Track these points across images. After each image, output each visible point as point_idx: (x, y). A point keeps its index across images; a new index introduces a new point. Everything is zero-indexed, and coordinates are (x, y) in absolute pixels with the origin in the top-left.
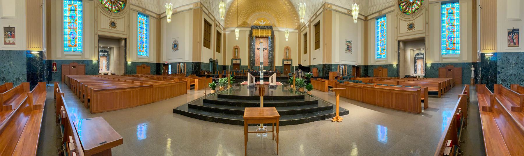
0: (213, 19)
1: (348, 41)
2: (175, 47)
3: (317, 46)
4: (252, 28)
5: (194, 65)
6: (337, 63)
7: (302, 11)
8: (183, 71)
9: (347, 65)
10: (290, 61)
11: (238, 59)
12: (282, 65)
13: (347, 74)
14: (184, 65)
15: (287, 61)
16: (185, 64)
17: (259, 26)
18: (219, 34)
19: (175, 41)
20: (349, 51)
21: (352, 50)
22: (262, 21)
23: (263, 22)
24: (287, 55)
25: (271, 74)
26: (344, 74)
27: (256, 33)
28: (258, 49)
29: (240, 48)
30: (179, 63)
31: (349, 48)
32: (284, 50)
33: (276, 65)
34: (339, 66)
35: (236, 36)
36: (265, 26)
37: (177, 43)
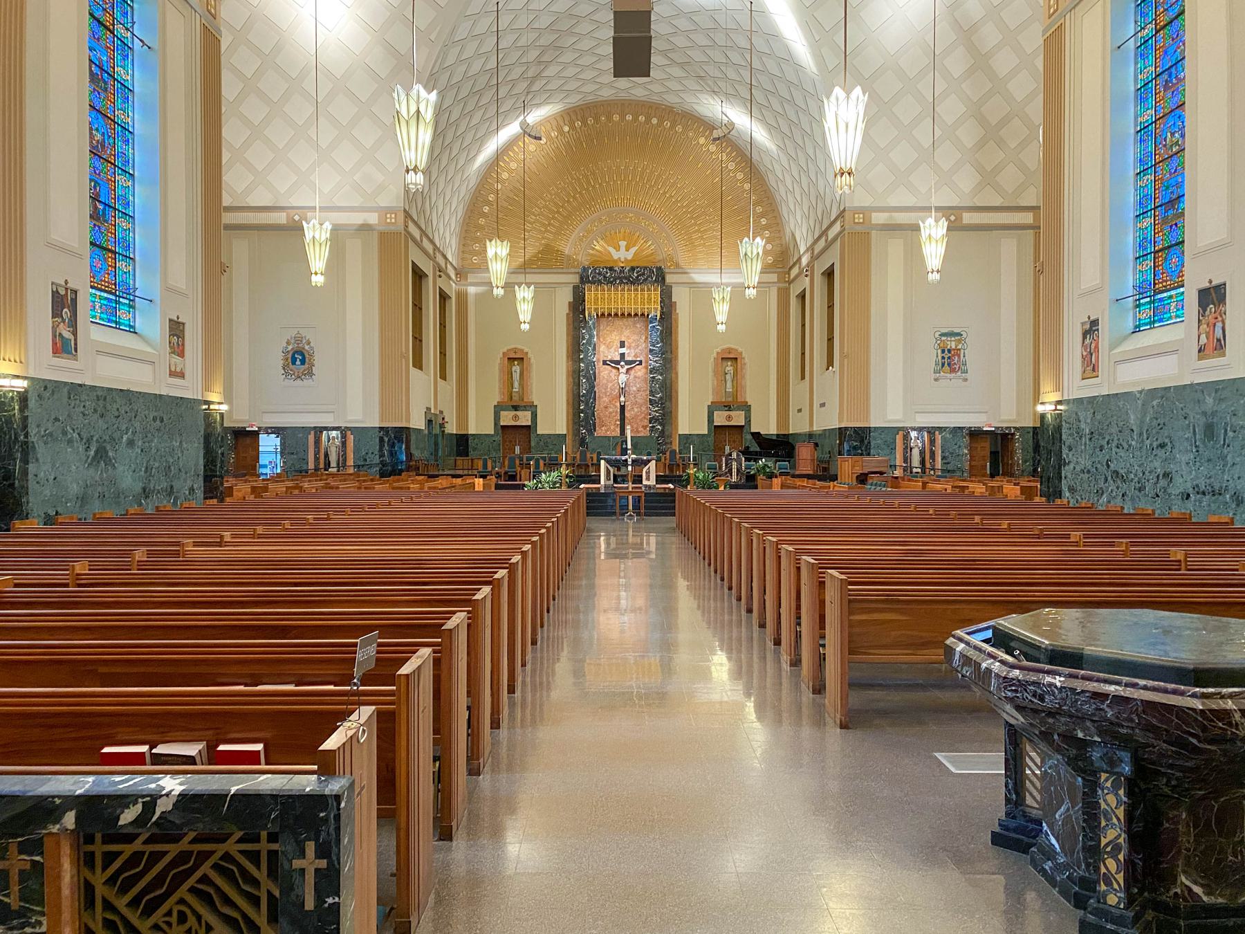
2: (298, 362)
3: (830, 363)
4: (584, 279)
5: (386, 439)
7: (749, 264)
8: (333, 464)
9: (940, 429)
11: (525, 408)
12: (706, 432)
13: (939, 464)
14: (344, 436)
15: (728, 413)
16: (349, 433)
17: (611, 269)
18: (444, 297)
19: (299, 339)
20: (953, 371)
22: (623, 244)
23: (627, 250)
26: (928, 465)
27: (596, 298)
28: (605, 363)
30: (319, 430)
31: (950, 360)
32: (716, 365)
33: (680, 432)
34: (901, 433)
35: (522, 318)
36: (633, 269)
37: (307, 347)
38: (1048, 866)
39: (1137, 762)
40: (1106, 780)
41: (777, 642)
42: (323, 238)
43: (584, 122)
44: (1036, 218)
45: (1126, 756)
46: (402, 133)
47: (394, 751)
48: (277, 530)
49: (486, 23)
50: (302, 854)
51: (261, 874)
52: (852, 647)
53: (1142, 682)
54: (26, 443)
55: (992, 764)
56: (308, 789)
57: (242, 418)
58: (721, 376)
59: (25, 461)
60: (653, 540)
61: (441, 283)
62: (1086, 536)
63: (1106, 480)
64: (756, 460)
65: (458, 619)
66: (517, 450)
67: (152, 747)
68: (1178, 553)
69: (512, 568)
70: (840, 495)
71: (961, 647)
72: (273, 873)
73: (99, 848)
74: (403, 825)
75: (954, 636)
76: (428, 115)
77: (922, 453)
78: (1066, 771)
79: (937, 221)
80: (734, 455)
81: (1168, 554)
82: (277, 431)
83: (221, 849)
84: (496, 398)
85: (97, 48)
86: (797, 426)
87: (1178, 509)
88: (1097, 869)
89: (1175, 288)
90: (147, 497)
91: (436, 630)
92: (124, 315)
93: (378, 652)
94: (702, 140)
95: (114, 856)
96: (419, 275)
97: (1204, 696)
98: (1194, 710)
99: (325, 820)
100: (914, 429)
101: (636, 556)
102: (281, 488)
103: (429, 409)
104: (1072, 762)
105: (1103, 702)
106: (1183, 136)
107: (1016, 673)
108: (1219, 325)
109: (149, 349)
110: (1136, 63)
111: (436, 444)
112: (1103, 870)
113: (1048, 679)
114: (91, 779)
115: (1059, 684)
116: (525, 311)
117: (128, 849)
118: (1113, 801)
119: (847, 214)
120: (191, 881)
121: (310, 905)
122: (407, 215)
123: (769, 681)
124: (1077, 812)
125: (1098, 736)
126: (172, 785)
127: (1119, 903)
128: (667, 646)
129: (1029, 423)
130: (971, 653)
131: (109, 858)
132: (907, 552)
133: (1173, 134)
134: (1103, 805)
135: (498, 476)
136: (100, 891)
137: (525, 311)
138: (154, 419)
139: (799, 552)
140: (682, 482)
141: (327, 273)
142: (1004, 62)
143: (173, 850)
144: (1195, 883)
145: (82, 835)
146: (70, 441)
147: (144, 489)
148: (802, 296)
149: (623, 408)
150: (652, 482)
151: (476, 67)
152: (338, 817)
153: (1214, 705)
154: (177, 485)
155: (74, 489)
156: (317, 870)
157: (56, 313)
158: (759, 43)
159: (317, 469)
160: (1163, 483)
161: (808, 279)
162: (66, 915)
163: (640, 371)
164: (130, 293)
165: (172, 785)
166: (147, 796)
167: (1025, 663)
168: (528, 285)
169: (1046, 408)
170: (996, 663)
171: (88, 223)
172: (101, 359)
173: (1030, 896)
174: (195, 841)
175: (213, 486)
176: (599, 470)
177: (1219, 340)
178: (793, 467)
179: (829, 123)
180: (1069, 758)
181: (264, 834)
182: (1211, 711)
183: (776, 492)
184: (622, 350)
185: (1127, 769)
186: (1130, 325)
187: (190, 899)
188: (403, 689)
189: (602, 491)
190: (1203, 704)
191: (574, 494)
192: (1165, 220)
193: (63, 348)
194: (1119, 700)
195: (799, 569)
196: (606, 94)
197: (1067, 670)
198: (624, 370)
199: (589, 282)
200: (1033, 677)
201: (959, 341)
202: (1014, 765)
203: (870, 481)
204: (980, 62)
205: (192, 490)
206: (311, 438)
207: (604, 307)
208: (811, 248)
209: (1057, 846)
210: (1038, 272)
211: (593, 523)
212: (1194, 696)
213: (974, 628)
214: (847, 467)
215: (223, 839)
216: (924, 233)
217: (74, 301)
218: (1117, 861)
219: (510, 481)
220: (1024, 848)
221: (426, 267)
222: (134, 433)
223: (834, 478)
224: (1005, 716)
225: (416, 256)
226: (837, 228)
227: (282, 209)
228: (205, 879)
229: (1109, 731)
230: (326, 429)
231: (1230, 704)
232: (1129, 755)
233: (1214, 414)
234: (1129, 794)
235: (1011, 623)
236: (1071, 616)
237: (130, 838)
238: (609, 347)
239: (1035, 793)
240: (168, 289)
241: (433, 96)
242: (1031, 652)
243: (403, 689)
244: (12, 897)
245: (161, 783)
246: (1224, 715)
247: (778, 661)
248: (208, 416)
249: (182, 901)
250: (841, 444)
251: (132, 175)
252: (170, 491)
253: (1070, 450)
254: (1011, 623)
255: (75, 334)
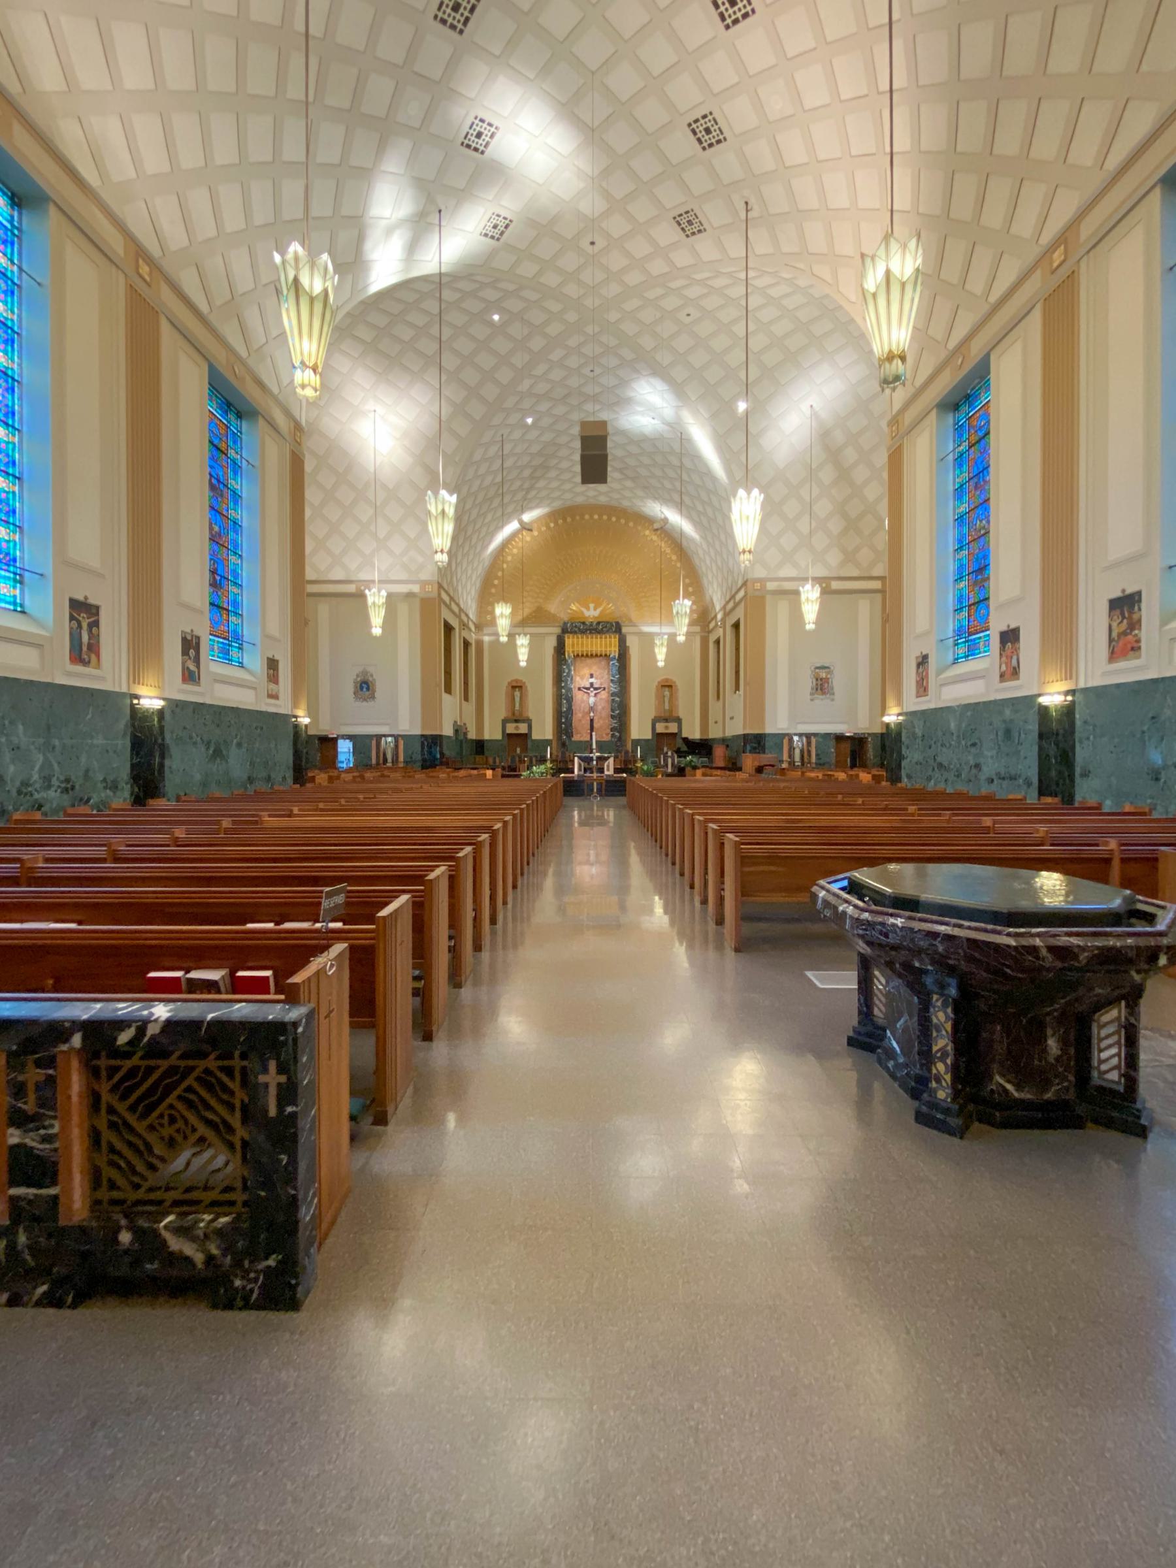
0: (117, 244)
1: (818, 665)
3: (737, 688)
4: (565, 630)
6: (782, 729)
8: (390, 760)
10: (676, 724)
11: (523, 721)
13: (814, 759)
14: (396, 741)
17: (584, 623)
18: (466, 644)
19: (365, 673)
21: (836, 690)
22: (592, 606)
23: (595, 609)
24: (667, 707)
25: (606, 759)
26: (806, 760)
27: (573, 644)
28: (579, 689)
29: (529, 687)
30: (379, 737)
31: (822, 686)
36: (599, 623)
37: (371, 679)
38: (891, 1064)
39: (961, 987)
40: (937, 1000)
41: (692, 887)
42: (381, 603)
43: (565, 520)
44: (884, 585)
45: (953, 982)
46: (432, 528)
47: (374, 976)
48: (335, 806)
49: (493, 450)
50: (265, 1070)
51: (235, 1085)
52: (745, 890)
53: (966, 923)
54: (163, 745)
55: (846, 981)
56: (271, 1017)
57: (325, 728)
58: (660, 698)
59: (163, 756)
60: (612, 813)
61: (465, 634)
62: (920, 809)
63: (933, 769)
64: (685, 757)
65: (440, 871)
66: (518, 750)
67: (187, 972)
68: (987, 821)
69: (494, 834)
70: (743, 780)
71: (822, 894)
72: (245, 1083)
73: (103, 1062)
74: (381, 1032)
75: (817, 885)
76: (450, 511)
77: (802, 751)
78: (905, 991)
79: (813, 586)
80: (670, 754)
81: (979, 822)
82: (350, 737)
83: (202, 1064)
84: (503, 714)
85: (216, 466)
86: (714, 733)
87: (985, 790)
88: (930, 1071)
89: (983, 631)
90: (251, 783)
91: (418, 879)
92: (234, 653)
93: (347, 897)
94: (647, 532)
95: (117, 1069)
96: (448, 629)
97: (1017, 935)
98: (1008, 946)
99: (285, 1043)
100: (796, 734)
101: (600, 824)
102: (348, 777)
103: (456, 722)
104: (910, 985)
105: (935, 939)
106: (988, 522)
107: (866, 915)
108: (1015, 658)
109: (43, 633)
110: (954, 471)
111: (461, 747)
112: (934, 1071)
113: (892, 920)
114: (98, 1006)
115: (900, 925)
116: (523, 655)
117: (128, 1064)
118: (942, 1017)
119: (748, 583)
120: (176, 1093)
121: (273, 1112)
122: (440, 586)
123: (687, 914)
124: (914, 1023)
125: (931, 965)
126: (161, 1011)
127: (947, 1098)
128: (623, 889)
129: (878, 730)
130: (831, 898)
131: (113, 1070)
132: (788, 821)
133: (981, 521)
134: (935, 1020)
135: (503, 768)
136: (106, 1097)
137: (523, 655)
138: (256, 728)
139: (707, 821)
140: (631, 772)
141: (384, 626)
142: (861, 474)
143: (164, 1064)
144: (1009, 1081)
145: (89, 1055)
146: (195, 743)
147: (249, 778)
148: (718, 642)
149: (592, 721)
150: (611, 772)
151: (489, 480)
152: (295, 1040)
153: (1024, 942)
154: (273, 776)
155: (198, 777)
156: (279, 1084)
157: (185, 652)
158: (687, 463)
159: (378, 764)
160: (974, 771)
161: (721, 630)
162: (75, 1119)
163: (604, 695)
164: (238, 638)
165: (161, 1011)
166: (139, 1021)
167: (874, 907)
168: (525, 635)
169: (892, 717)
170: (850, 907)
171: (207, 589)
172: (217, 686)
173: (877, 1085)
174: (181, 1057)
175: (299, 774)
176: (573, 765)
177: (1014, 668)
178: (711, 761)
179: (735, 516)
180: (908, 982)
181: (237, 1054)
182: (1023, 947)
183: (700, 780)
184: (592, 680)
185: (953, 991)
186: (950, 658)
187: (180, 1106)
188: (381, 928)
189: (576, 779)
190: (1016, 941)
191: (555, 779)
192: (975, 583)
193: (190, 677)
194: (949, 938)
195: (706, 833)
196: (580, 500)
197: (908, 914)
198: (593, 694)
199: (568, 632)
200: (880, 919)
201: (828, 673)
202: (865, 984)
203: (765, 771)
204: (843, 475)
205: (284, 778)
206: (374, 742)
207: (579, 649)
208: (724, 608)
209: (898, 1049)
210: (885, 621)
211: (568, 801)
212: (1009, 935)
213: (833, 878)
214: (749, 761)
215: (204, 1055)
216: (803, 597)
217: (198, 644)
218: (946, 1064)
219: (511, 772)
220: (869, 1048)
221: (454, 622)
222: (241, 738)
223: (740, 769)
224: (858, 948)
225: (446, 615)
226: (741, 594)
227: (350, 582)
228: (189, 1089)
229: (941, 962)
230: (385, 736)
231: (1038, 942)
232: (955, 981)
233: (1012, 721)
234: (956, 1011)
235: (863, 875)
236: (909, 868)
237: (128, 1055)
238: (582, 678)
239: (881, 1006)
240: (267, 636)
241: (454, 499)
242: (878, 898)
243: (381, 928)
244: (29, 1104)
245: (153, 1010)
246: (1034, 950)
247: (692, 900)
248: (296, 726)
249: (171, 1106)
250: (745, 745)
251: (241, 556)
252: (268, 779)
253: (908, 748)
254: (863, 875)
255: (198, 667)
